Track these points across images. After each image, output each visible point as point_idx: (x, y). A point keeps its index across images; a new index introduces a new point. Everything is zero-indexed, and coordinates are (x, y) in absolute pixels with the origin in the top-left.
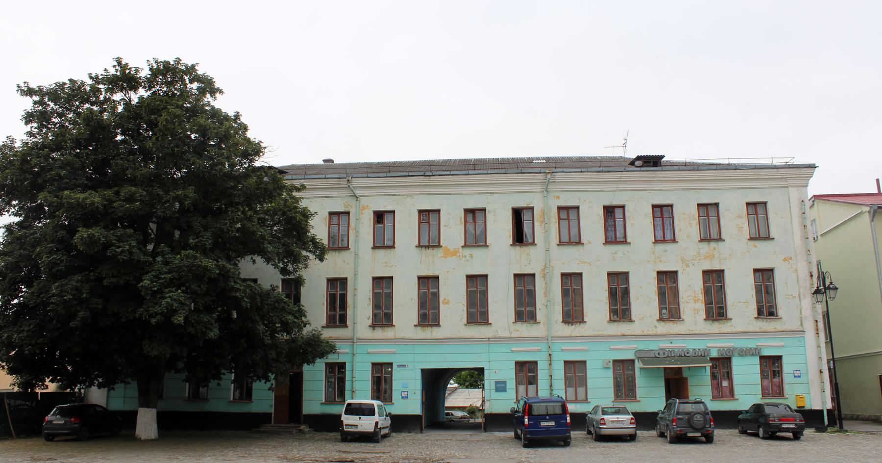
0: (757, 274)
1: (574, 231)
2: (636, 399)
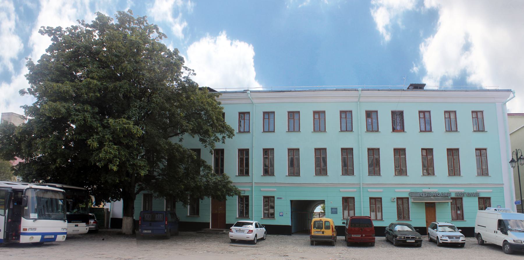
0: (477, 151)
1: (349, 125)
2: (409, 220)
